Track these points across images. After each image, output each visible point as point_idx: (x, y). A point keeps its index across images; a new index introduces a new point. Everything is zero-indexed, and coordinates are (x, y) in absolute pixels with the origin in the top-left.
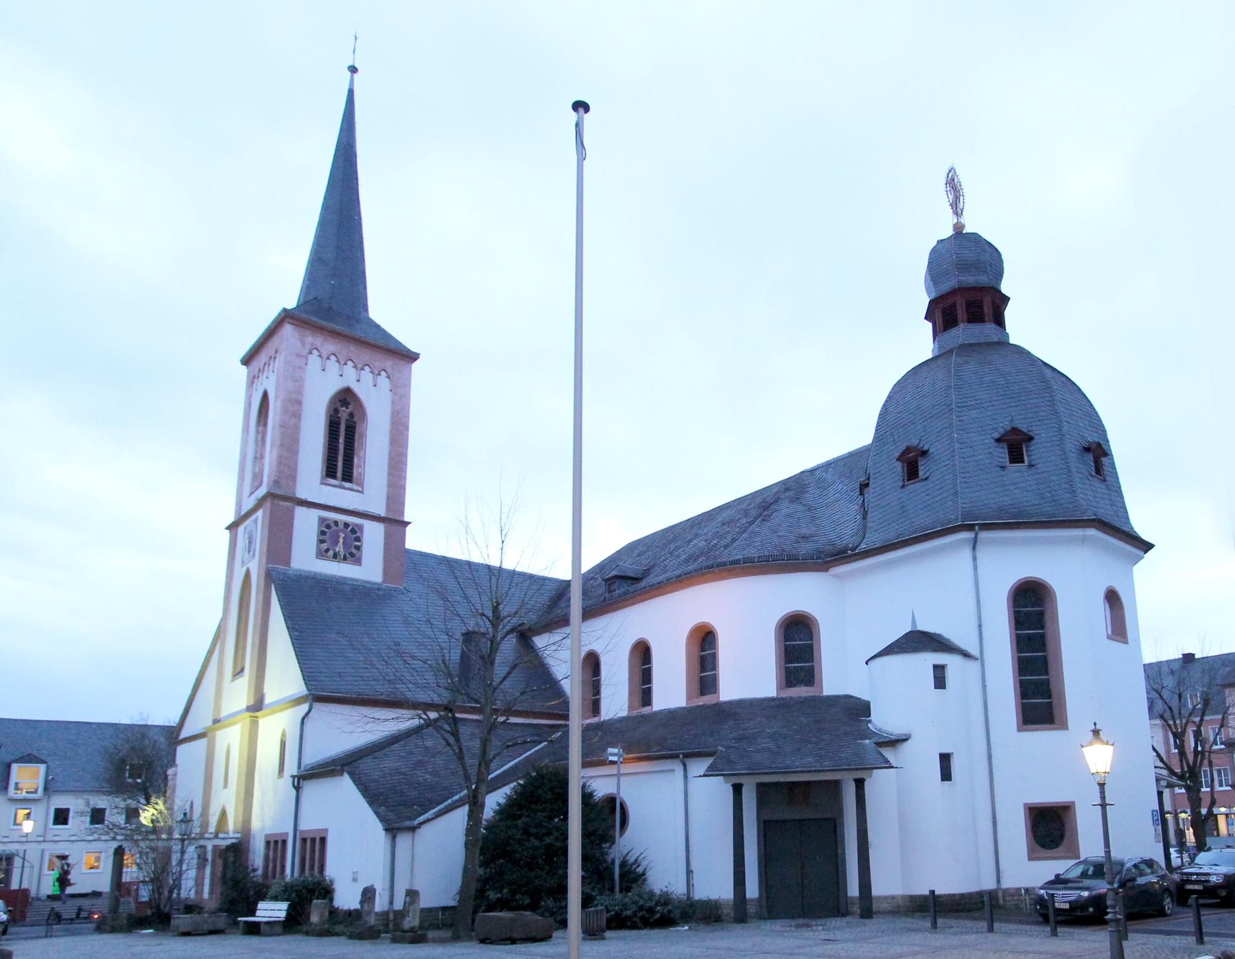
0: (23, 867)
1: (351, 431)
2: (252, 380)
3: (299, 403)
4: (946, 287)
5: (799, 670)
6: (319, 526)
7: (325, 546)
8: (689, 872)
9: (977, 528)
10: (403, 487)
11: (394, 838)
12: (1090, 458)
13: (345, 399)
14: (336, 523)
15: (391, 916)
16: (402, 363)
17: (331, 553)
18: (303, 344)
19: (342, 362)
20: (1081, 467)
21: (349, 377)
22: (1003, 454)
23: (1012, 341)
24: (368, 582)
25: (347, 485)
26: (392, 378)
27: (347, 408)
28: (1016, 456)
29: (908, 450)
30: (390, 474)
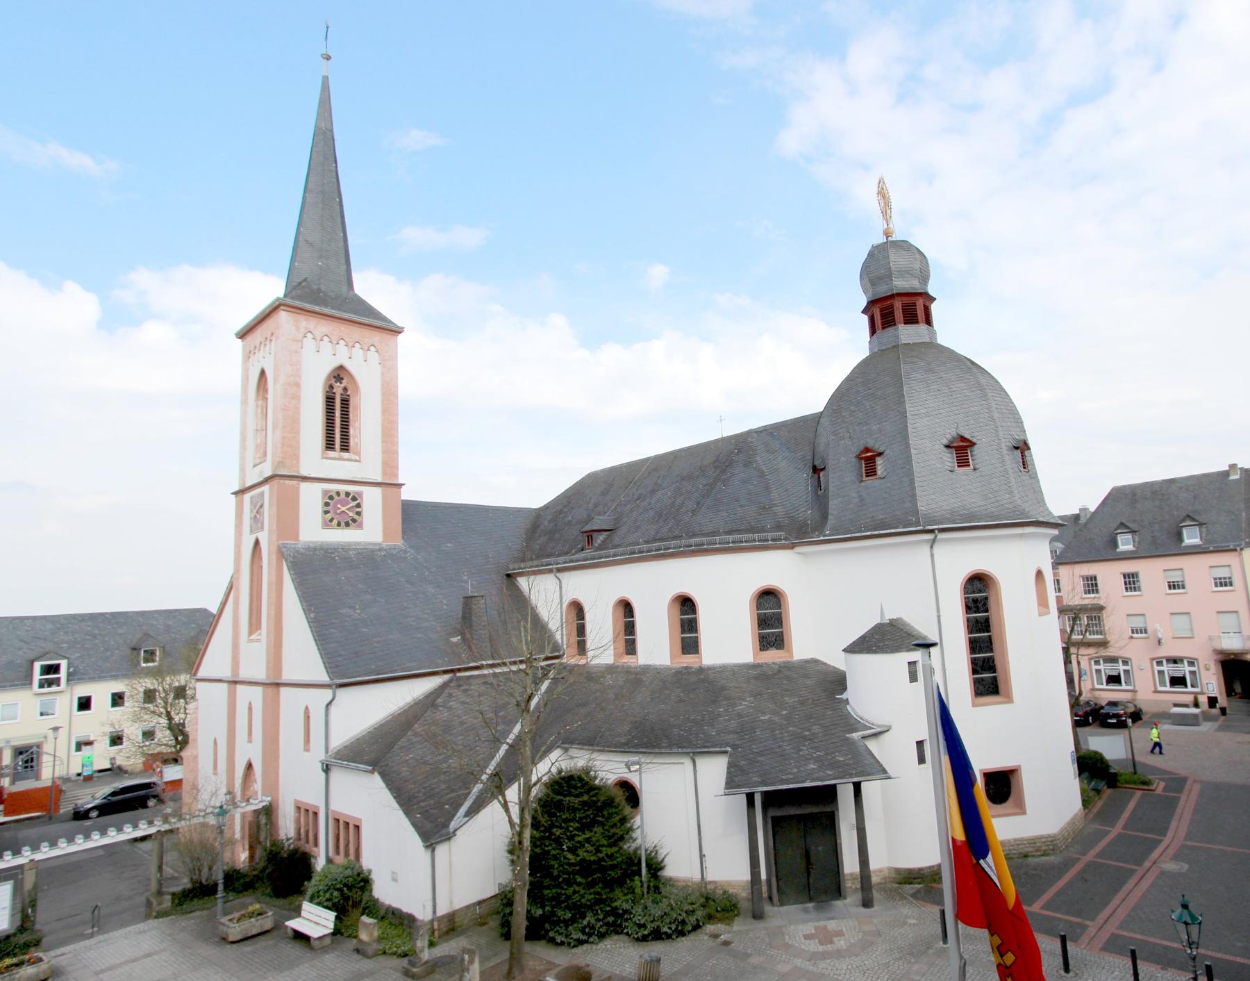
0: (54, 766)
1: (345, 403)
2: (248, 356)
3: (298, 385)
5: (770, 635)
6: (323, 498)
7: (329, 516)
8: (702, 856)
9: (936, 531)
10: (396, 452)
11: (433, 851)
13: (339, 374)
14: (338, 494)
15: (436, 924)
16: (389, 336)
17: (335, 522)
18: (298, 328)
19: (335, 342)
20: (1012, 459)
21: (342, 356)
22: (949, 458)
24: (370, 544)
25: (345, 455)
26: (380, 352)
27: (341, 383)
28: (963, 462)
30: (383, 442)
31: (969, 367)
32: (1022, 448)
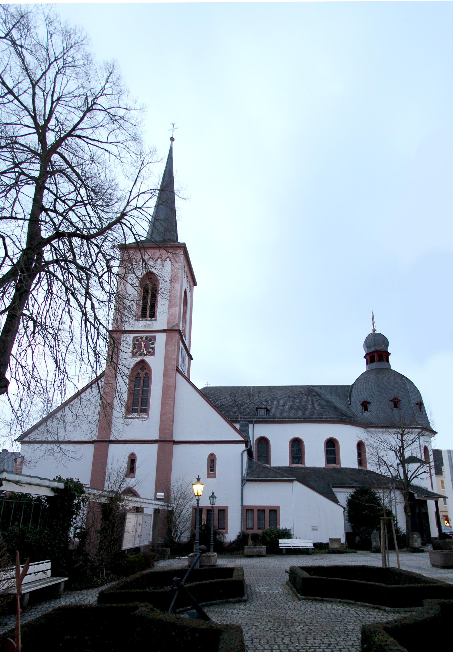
4: (372, 349)
7: (135, 350)
12: (418, 407)
14: (142, 338)
23: (392, 368)
29: (364, 402)
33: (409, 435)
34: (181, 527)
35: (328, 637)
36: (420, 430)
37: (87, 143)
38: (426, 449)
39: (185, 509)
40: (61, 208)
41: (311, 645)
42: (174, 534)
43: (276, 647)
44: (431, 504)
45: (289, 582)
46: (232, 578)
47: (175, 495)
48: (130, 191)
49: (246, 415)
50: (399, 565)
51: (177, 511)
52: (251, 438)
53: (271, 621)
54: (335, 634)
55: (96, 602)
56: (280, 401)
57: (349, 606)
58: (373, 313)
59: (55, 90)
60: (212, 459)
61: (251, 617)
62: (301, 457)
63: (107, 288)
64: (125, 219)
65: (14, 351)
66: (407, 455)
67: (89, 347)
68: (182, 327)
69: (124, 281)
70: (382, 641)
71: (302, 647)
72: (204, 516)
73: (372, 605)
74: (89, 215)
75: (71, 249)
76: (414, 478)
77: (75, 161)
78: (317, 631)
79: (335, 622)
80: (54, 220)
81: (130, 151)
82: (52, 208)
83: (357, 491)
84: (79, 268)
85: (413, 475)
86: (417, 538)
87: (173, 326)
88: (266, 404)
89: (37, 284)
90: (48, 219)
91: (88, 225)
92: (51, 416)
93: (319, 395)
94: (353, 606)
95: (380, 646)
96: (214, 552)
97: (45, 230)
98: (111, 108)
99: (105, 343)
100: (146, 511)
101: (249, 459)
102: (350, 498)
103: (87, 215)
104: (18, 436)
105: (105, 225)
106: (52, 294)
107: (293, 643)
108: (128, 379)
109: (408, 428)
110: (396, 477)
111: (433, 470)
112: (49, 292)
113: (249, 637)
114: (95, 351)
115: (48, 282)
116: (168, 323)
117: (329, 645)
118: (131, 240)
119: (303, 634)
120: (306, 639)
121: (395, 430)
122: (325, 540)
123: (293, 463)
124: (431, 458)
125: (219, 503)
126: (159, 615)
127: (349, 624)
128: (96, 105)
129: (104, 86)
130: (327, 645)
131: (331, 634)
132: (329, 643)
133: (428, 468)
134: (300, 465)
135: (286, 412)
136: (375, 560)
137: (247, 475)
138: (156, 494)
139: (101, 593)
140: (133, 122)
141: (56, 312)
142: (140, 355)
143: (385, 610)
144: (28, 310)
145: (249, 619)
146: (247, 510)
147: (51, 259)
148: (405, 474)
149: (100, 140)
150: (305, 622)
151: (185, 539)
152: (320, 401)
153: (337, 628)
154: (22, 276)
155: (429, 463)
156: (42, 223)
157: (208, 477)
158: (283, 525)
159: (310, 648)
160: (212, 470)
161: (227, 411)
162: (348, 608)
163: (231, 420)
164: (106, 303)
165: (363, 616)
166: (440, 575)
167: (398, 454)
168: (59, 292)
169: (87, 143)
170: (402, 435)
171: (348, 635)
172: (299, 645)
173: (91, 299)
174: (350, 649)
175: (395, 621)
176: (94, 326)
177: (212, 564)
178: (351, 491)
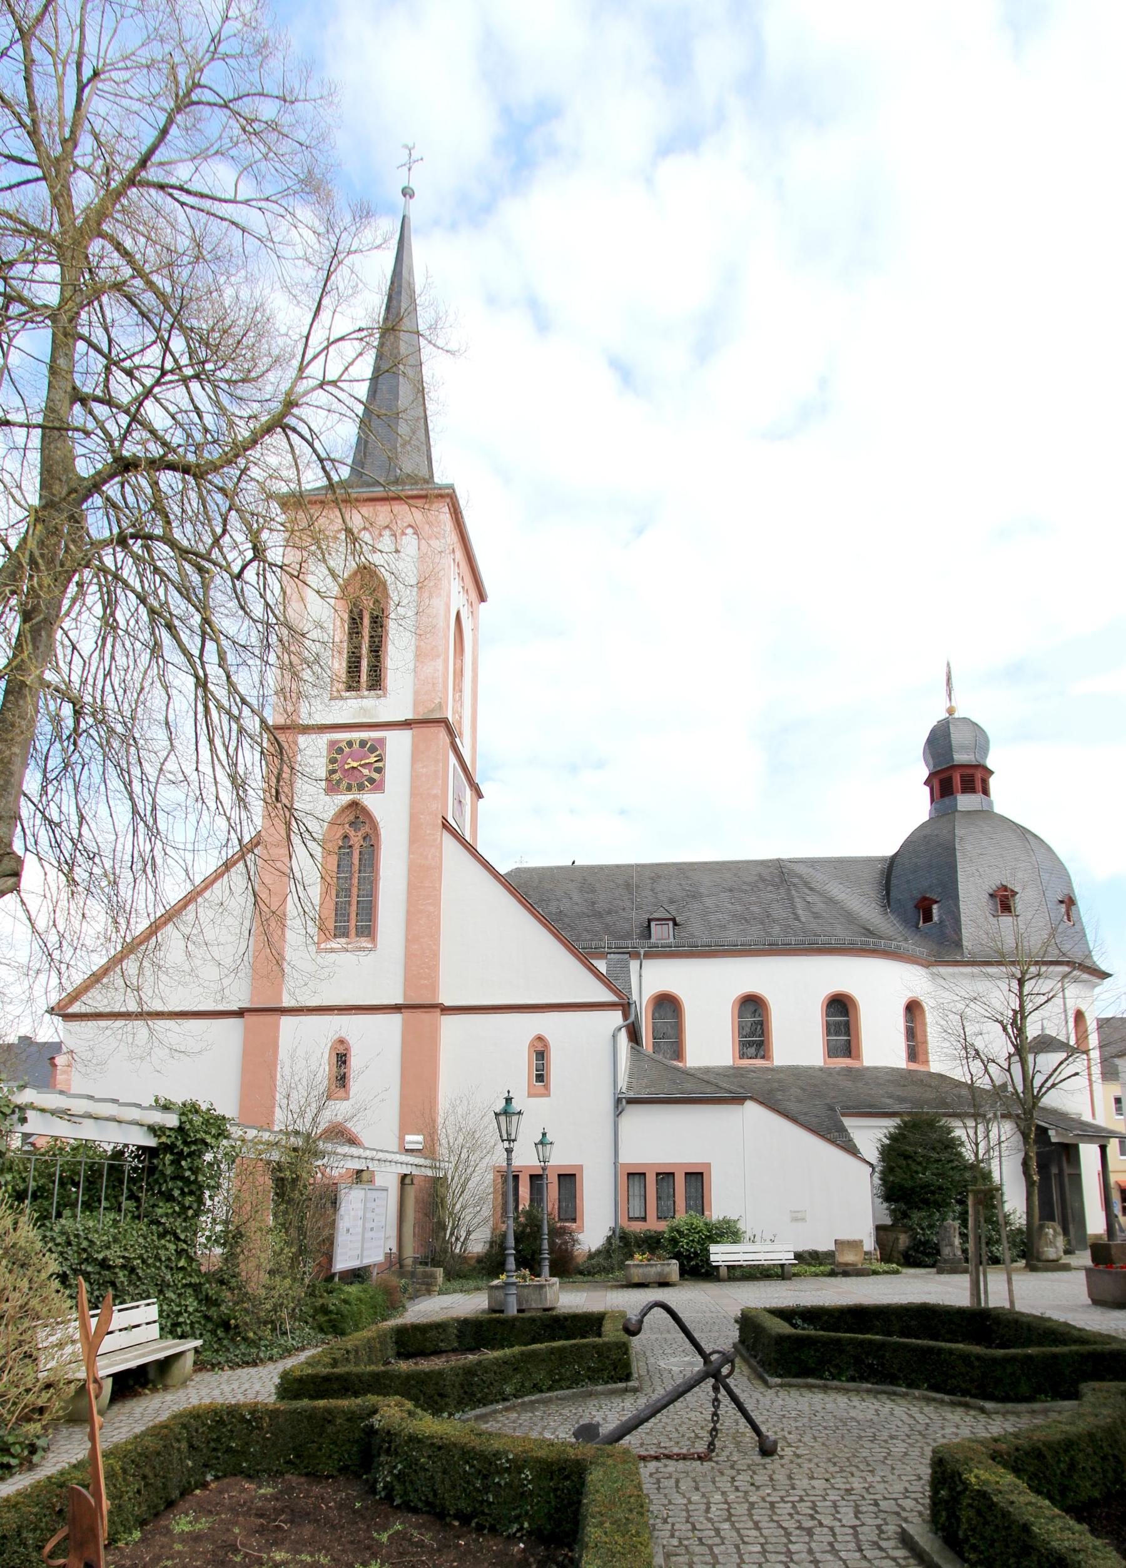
7: (336, 777)
12: (1063, 908)
14: (350, 744)
31: (1023, 833)
32: (1069, 902)
33: (1041, 981)
34: (468, 1218)
35: (844, 1474)
36: (1067, 969)
37: (183, 204)
38: (1079, 1016)
39: (476, 1174)
40: (124, 390)
41: (803, 1493)
42: (452, 1234)
43: (718, 1497)
44: (1089, 1154)
45: (740, 1346)
46: (599, 1335)
47: (451, 1141)
48: (305, 334)
49: (622, 938)
50: (1012, 1302)
51: (456, 1178)
52: (635, 997)
53: (702, 1438)
54: (862, 1466)
55: (275, 1397)
56: (709, 902)
57: (893, 1401)
58: (948, 665)
59: (86, 49)
60: (541, 1053)
61: (651, 1429)
62: (762, 1041)
63: (258, 610)
64: (295, 416)
65: (31, 782)
66: (1032, 1031)
67: (218, 767)
68: (454, 713)
69: (300, 583)
70: (986, 1482)
71: (782, 1498)
72: (524, 1191)
73: (947, 1398)
74: (197, 410)
75: (158, 507)
76: (1049, 1089)
77: (151, 256)
78: (816, 1460)
79: (860, 1437)
80: (108, 425)
81: (299, 224)
82: (99, 393)
83: (905, 1123)
84: (183, 553)
85: (1046, 1081)
86: (1055, 1236)
87: (432, 711)
88: (672, 908)
89: (74, 601)
90: (91, 425)
91: (198, 436)
92: (130, 949)
93: (806, 884)
94: (900, 1401)
95: (983, 1495)
96: (552, 1275)
97: (84, 455)
98: (240, 98)
99: (257, 756)
100: (379, 1181)
101: (632, 1048)
102: (888, 1142)
103: (191, 408)
104: (54, 998)
105: (244, 432)
106: (115, 628)
107: (758, 1488)
108: (320, 849)
109: (1037, 963)
110: (1005, 1085)
111: (1096, 1070)
112: (107, 624)
113: (651, 1475)
114: (233, 778)
115: (102, 598)
116: (416, 704)
117: (849, 1491)
118: (313, 479)
119: (782, 1466)
120: (790, 1478)
121: (1003, 969)
122: (825, 1245)
123: (742, 1056)
124: (1093, 1040)
125: (560, 1158)
126: (429, 1425)
127: (895, 1441)
128: (199, 90)
129: (220, 32)
130: (842, 1492)
131: (851, 1465)
132: (848, 1486)
133: (1086, 1062)
134: (759, 1063)
135: (723, 927)
136: (950, 1289)
137: (629, 1088)
138: (402, 1139)
139: (284, 1376)
140: (301, 136)
141: (128, 677)
142: (349, 788)
143: (982, 1410)
144: (57, 669)
145: (647, 1433)
146: (629, 1174)
147: (107, 534)
148: (1027, 1080)
149: (219, 195)
150: (784, 1438)
151: (477, 1246)
152: (809, 899)
153: (865, 1453)
154: (35, 579)
155: (1086, 1052)
156: (77, 435)
157: (530, 1095)
158: (719, 1209)
159: (802, 1500)
160: (540, 1078)
161: (573, 929)
162: (889, 1405)
163: (584, 956)
164: (257, 652)
165: (927, 1424)
166: (1113, 1325)
167: (1010, 1031)
168: (132, 622)
169: (183, 204)
170: (1021, 983)
171: (893, 1469)
172: (775, 1493)
173: (217, 641)
174: (900, 1501)
175: (1016, 1436)
176: (229, 713)
177: (548, 1305)
178: (890, 1124)
